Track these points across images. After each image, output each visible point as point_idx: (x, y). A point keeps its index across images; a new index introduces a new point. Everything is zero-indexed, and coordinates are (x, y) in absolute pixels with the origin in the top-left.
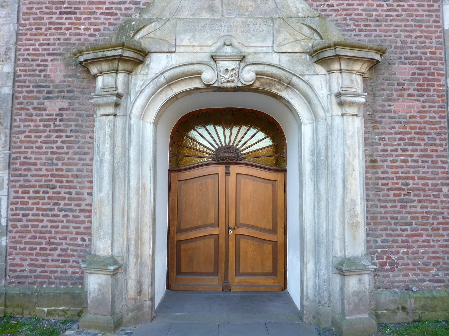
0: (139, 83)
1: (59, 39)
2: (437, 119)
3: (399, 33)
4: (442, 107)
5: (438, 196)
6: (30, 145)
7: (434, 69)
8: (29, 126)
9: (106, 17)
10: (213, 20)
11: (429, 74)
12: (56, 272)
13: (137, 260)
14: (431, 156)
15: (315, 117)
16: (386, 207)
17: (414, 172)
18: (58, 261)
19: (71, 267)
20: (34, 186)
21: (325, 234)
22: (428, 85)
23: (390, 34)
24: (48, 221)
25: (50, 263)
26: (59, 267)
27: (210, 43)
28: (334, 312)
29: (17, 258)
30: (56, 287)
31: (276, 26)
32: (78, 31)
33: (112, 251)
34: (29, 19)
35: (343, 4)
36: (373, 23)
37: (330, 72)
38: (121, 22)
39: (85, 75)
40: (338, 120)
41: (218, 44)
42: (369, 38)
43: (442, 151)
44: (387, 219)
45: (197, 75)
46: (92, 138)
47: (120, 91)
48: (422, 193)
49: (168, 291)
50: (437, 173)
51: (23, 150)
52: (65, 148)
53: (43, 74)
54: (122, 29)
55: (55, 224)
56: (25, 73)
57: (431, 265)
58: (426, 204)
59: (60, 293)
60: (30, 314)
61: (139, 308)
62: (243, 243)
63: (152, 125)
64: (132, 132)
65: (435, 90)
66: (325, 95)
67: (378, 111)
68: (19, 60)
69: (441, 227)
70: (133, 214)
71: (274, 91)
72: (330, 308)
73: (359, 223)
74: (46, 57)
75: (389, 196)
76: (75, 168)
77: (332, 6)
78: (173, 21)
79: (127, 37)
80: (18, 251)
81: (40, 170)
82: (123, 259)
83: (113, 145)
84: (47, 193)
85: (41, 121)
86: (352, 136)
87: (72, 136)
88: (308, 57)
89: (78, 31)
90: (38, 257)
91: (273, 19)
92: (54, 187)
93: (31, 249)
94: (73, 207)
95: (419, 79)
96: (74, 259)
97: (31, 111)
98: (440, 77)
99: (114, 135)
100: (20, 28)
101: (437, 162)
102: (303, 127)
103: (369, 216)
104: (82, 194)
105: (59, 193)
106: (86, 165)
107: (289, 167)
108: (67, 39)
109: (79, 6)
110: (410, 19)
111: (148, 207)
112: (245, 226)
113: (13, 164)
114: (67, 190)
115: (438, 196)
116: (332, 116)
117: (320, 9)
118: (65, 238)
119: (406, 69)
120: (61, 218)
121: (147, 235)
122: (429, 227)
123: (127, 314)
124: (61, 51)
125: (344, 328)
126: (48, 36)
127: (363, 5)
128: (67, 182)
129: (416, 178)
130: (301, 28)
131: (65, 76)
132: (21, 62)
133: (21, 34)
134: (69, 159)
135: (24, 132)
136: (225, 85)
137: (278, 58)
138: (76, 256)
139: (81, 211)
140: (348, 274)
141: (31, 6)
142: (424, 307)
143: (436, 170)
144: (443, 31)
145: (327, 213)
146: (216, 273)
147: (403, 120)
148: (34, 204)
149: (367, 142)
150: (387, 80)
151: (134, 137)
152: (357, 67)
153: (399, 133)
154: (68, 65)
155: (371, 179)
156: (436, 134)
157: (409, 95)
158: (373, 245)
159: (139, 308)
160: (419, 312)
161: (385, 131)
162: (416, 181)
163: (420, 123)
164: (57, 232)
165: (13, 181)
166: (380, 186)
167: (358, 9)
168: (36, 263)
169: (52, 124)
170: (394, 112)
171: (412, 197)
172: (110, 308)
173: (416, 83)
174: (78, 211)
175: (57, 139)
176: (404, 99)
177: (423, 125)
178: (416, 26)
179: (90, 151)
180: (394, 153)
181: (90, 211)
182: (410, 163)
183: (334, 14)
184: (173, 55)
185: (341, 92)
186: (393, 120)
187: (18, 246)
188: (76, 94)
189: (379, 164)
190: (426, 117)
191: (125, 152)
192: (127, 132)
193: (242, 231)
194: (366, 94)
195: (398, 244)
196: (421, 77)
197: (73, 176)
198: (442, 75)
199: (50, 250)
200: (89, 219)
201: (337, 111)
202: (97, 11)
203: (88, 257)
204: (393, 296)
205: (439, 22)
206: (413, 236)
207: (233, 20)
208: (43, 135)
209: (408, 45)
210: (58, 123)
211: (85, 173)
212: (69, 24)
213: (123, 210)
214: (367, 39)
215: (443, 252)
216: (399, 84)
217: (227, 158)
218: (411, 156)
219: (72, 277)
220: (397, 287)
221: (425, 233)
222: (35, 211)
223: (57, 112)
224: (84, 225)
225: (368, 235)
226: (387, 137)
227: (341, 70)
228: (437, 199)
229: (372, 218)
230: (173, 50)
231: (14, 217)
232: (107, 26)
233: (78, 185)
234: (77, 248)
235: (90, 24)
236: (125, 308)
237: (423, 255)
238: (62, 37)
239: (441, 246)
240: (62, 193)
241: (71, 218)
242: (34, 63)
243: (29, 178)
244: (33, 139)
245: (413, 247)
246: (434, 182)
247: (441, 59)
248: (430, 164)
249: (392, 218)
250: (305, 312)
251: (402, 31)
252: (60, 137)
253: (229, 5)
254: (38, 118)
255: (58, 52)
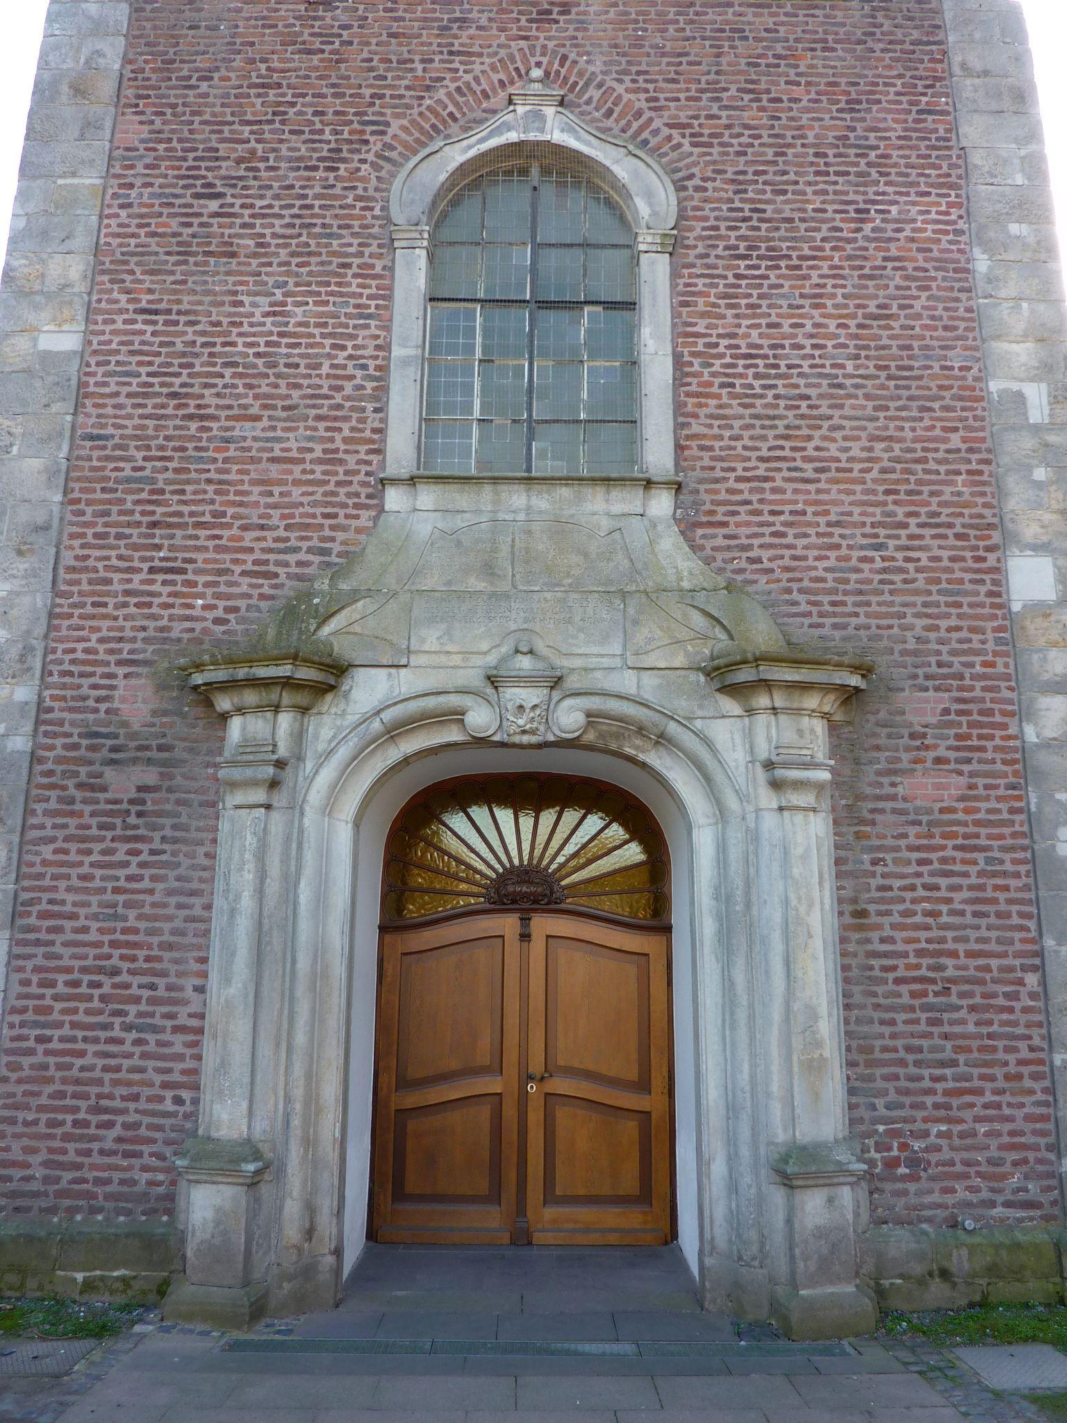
0: (326, 733)
1: (144, 629)
2: (1005, 816)
3: (909, 620)
4: (1013, 787)
5: (1014, 996)
6: (64, 870)
7: (992, 701)
8: (65, 826)
9: (254, 581)
10: (493, 595)
11: (981, 713)
12: (108, 1182)
13: (306, 1151)
14: (995, 901)
15: (721, 813)
16: (892, 1022)
17: (955, 939)
18: (114, 1153)
19: (145, 1169)
20: (69, 970)
21: (748, 1088)
22: (980, 737)
23: (890, 622)
24: (96, 1054)
25: (97, 1159)
26: (117, 1168)
27: (485, 646)
28: (772, 1280)
29: (16, 1146)
30: (107, 1219)
31: (631, 611)
32: (188, 612)
33: (249, 1127)
34: (78, 582)
35: (782, 557)
36: (850, 599)
37: (751, 712)
38: (287, 592)
39: (200, 711)
40: (770, 821)
41: (504, 650)
42: (843, 633)
43: (1019, 889)
44: (896, 1051)
45: (456, 716)
46: (211, 856)
47: (282, 751)
48: (978, 989)
49: (371, 1244)
50: (1012, 943)
51: (47, 882)
52: (147, 879)
53: (103, 707)
54: (291, 614)
55: (113, 1062)
56: (63, 704)
57: (1008, 1164)
58: (987, 1016)
59: (117, 1235)
60: (41, 1288)
61: (308, 1271)
62: (563, 1115)
63: (350, 825)
64: (306, 845)
65: (996, 749)
66: (742, 762)
67: (865, 798)
68: (51, 674)
69: (1025, 1070)
70: (300, 1038)
71: (629, 751)
72: (764, 1271)
73: (825, 1060)
74: (113, 669)
75: (899, 995)
76: (166, 926)
77: (759, 560)
78: (404, 598)
79: (301, 632)
80: (19, 1129)
81: (85, 930)
82: (274, 1149)
83: (262, 876)
84: (99, 985)
85: (93, 814)
86: (805, 858)
87: (164, 852)
88: (702, 678)
89: (188, 612)
90: (66, 1145)
91: (624, 595)
92: (115, 972)
93: (52, 1124)
94: (157, 1021)
95: (960, 724)
96: (154, 1148)
97: (72, 791)
98: (1006, 720)
99: (264, 853)
100: (58, 601)
101: (1008, 915)
102: (695, 832)
103: (854, 1044)
104: (181, 989)
105: (127, 986)
106: (193, 919)
107: (679, 918)
108: (162, 630)
109: (193, 556)
110: (934, 588)
111: (334, 1022)
112: (570, 1072)
113: (21, 915)
114: (146, 980)
115: (1014, 996)
116: (758, 811)
117: (730, 567)
118: (135, 1098)
119: (927, 701)
120: (127, 1047)
121: (330, 1090)
122: (998, 1072)
123: (281, 1287)
124: (148, 655)
125: (795, 1317)
126: (121, 622)
127: (827, 558)
128: (148, 959)
129: (962, 954)
130: (685, 615)
131: (154, 713)
132: (55, 678)
133: (59, 616)
134: (154, 905)
135: (53, 840)
136: (516, 739)
137: (635, 680)
138: (160, 1142)
139: (177, 1029)
140: (800, 1183)
141: (86, 552)
142: (992, 1270)
143: (1008, 934)
144: (1009, 615)
145: (752, 1039)
146: (494, 1196)
147: (925, 819)
148: (64, 1011)
149: (844, 868)
150: (885, 726)
151: (309, 856)
152: (812, 701)
153: (918, 849)
154: (162, 687)
155: (855, 955)
156: (1003, 849)
157: (938, 761)
158: (867, 1115)
159: (308, 1271)
160: (983, 1282)
161: (885, 842)
162: (963, 960)
163: (966, 824)
164: (115, 1083)
165: (18, 957)
166: (877, 973)
167: (816, 568)
168: (60, 1158)
169: (118, 821)
170: (905, 799)
171: (954, 999)
172: (240, 1266)
173: (952, 732)
174: (169, 1030)
175: (128, 858)
176: (925, 769)
177: (971, 829)
178: (947, 604)
179: (203, 886)
180: (908, 895)
181: (200, 1031)
182: (945, 919)
183: (763, 579)
184: (403, 671)
185: (774, 759)
186: (903, 818)
187: (20, 1115)
188: (178, 753)
189: (874, 919)
190: (978, 810)
191: (287, 890)
192: (294, 846)
193: (560, 1085)
194: (832, 762)
195: (925, 1113)
196: (963, 719)
197: (162, 946)
198: (1012, 714)
199: (98, 1127)
200: (195, 1051)
201: (769, 800)
202: (233, 567)
203: (189, 1143)
204: (918, 1242)
205: (999, 595)
206: (961, 1092)
207: (535, 596)
208: (97, 847)
209: (930, 646)
210: (132, 820)
211: (190, 939)
212: (169, 595)
213: (279, 1029)
214: (837, 634)
215: (1035, 1133)
216: (912, 736)
217: (525, 896)
218: (949, 901)
219: (146, 1194)
220: (929, 1220)
221: (989, 1085)
222: (66, 1031)
223: (133, 794)
224: (181, 1066)
225: (852, 1091)
226: (889, 857)
227: (774, 708)
228: (1013, 1003)
229: (861, 1050)
230: (404, 661)
231: (15, 1045)
232: (254, 601)
233: (173, 968)
234: (162, 1121)
235: (218, 596)
236: (275, 1270)
237: (987, 1141)
238: (151, 624)
239: (1029, 1118)
240: (135, 986)
241: (151, 1047)
242: (86, 682)
243: (58, 949)
244: (73, 857)
245: (961, 1121)
246: (1005, 962)
247: (1007, 678)
248: (993, 920)
249: (909, 1049)
250: (708, 1285)
251: (917, 615)
252: (137, 853)
253: (527, 563)
254: (88, 809)
255: (141, 657)
